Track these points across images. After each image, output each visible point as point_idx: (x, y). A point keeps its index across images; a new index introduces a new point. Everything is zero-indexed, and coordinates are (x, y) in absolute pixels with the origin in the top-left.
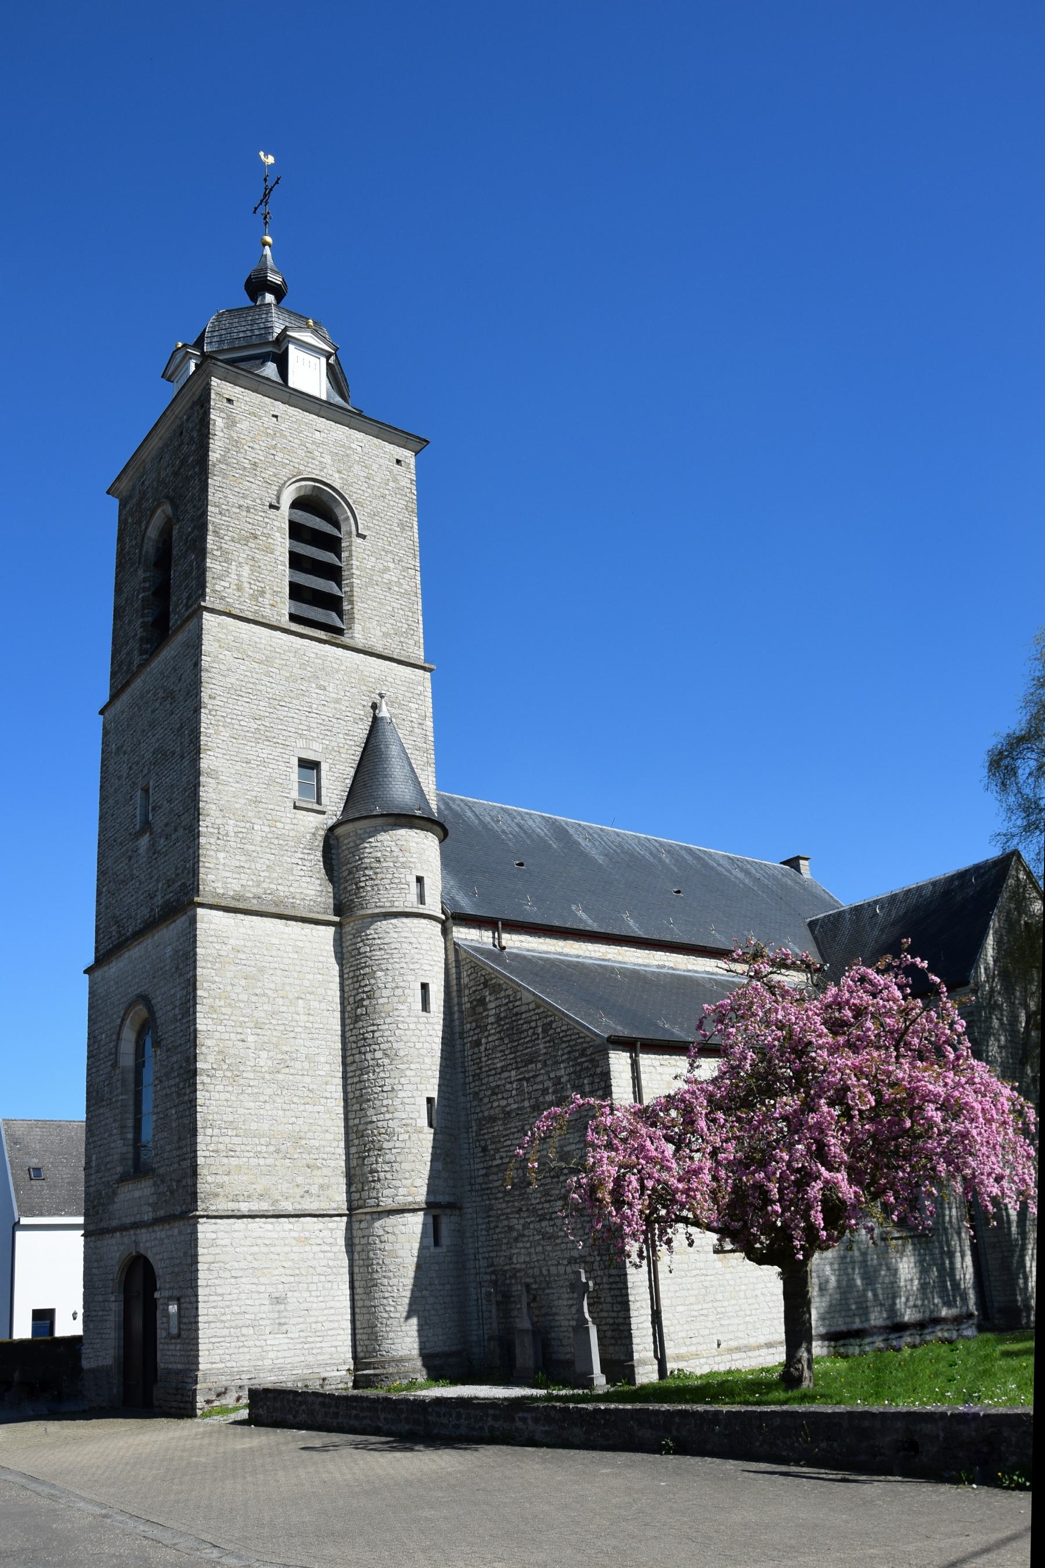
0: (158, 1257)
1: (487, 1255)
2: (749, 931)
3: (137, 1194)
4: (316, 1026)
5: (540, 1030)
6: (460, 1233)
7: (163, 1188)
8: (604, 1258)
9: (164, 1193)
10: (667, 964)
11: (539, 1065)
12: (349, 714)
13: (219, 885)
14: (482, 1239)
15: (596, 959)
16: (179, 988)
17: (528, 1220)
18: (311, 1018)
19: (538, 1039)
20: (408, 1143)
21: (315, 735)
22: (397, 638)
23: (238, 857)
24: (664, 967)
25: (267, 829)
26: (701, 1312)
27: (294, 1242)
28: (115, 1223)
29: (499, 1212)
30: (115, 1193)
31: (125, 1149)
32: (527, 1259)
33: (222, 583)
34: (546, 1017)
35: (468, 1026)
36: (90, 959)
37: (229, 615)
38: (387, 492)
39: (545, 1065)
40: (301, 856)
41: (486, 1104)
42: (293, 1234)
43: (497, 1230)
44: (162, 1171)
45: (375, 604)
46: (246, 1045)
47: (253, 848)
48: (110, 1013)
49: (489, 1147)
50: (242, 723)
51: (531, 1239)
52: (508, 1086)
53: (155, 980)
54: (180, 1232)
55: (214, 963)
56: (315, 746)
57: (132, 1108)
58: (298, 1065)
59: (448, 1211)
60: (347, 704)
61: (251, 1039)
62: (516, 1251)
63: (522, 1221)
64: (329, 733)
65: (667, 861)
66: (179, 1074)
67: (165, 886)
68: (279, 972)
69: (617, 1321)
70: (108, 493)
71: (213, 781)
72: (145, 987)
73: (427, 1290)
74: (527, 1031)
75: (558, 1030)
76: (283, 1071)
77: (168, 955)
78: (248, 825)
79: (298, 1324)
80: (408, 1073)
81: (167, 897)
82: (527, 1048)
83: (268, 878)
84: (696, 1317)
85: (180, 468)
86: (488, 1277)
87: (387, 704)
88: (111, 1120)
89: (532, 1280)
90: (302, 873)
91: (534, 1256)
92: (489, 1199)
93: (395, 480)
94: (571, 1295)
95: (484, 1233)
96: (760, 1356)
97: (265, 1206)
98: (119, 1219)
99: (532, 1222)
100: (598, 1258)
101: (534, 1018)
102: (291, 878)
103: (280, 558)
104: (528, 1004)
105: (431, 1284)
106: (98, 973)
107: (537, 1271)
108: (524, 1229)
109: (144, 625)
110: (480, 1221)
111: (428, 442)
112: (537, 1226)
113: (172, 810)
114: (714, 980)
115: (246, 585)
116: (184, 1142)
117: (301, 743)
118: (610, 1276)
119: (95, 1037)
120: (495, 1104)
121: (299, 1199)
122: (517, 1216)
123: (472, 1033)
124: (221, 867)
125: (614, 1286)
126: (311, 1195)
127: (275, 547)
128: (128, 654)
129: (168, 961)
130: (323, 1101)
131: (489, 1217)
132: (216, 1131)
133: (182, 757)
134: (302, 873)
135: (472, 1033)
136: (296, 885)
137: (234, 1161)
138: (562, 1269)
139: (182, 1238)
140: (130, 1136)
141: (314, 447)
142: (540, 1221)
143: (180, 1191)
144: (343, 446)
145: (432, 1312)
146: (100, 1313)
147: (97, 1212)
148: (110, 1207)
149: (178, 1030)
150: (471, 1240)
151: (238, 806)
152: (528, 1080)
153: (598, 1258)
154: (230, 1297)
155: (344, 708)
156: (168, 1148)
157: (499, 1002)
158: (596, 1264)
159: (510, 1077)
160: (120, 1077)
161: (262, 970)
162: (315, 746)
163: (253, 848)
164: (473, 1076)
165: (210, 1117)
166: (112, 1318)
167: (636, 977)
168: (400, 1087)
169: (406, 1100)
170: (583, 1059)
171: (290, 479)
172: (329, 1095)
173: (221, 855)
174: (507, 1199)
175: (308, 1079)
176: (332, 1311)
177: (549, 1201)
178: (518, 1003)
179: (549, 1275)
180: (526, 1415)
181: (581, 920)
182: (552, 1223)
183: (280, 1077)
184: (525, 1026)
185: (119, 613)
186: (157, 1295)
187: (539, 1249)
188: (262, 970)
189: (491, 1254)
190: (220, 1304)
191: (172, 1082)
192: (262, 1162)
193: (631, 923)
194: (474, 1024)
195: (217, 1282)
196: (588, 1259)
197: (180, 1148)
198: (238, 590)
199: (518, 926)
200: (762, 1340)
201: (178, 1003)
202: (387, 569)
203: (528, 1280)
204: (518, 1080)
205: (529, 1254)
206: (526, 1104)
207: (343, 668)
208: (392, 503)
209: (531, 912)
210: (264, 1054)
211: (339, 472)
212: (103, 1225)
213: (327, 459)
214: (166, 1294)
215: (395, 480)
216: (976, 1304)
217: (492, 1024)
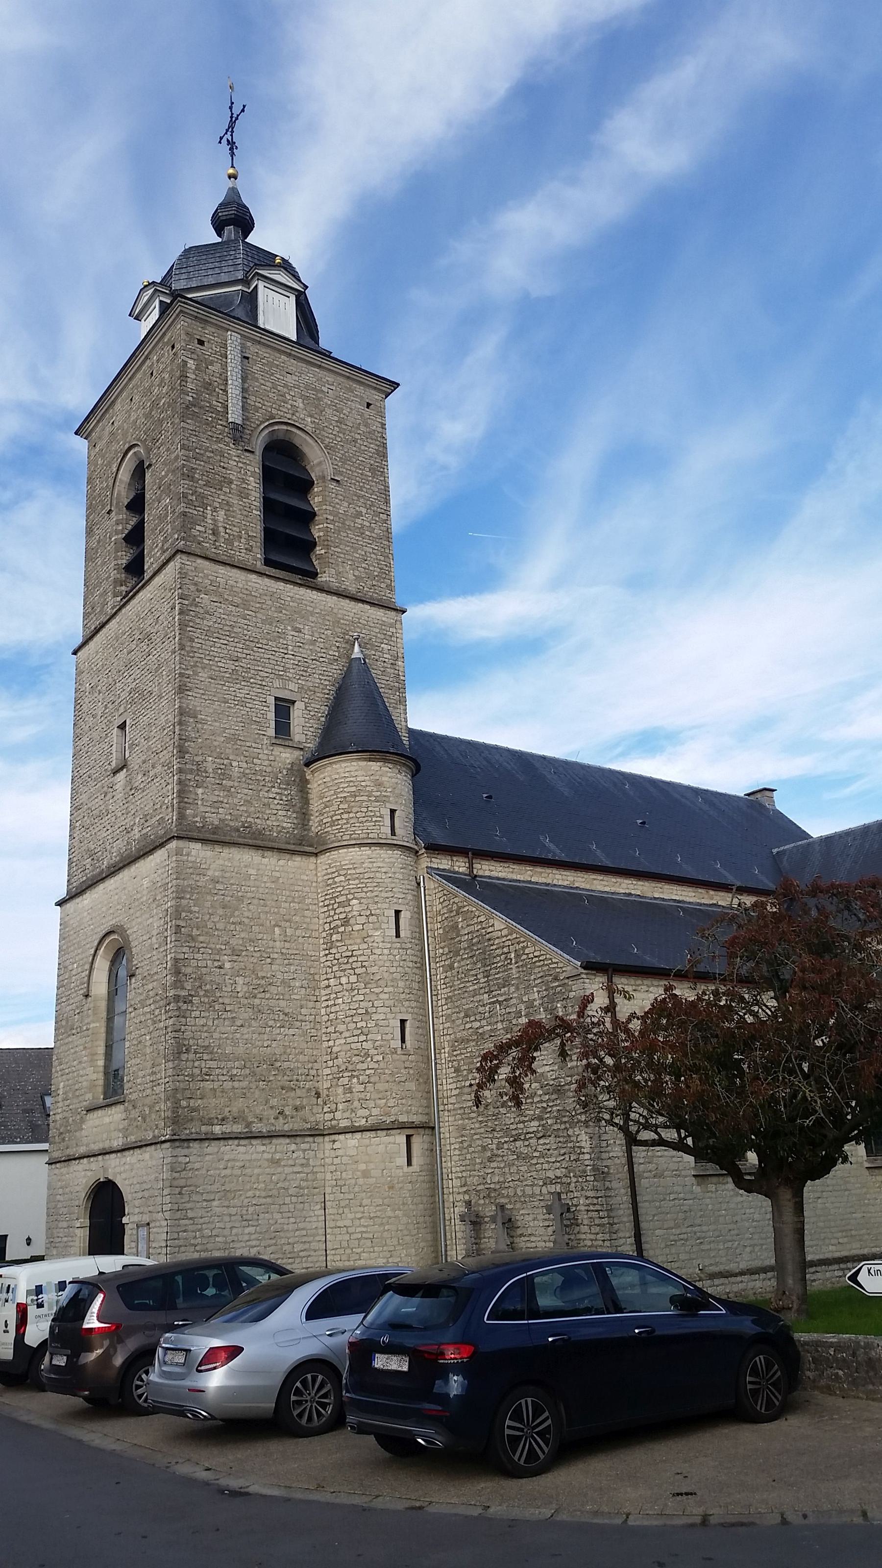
0: (127, 1182)
2: (715, 861)
3: (107, 1120)
4: (290, 952)
5: (513, 955)
7: (135, 1114)
9: (135, 1119)
10: (633, 892)
11: (512, 989)
12: (324, 655)
13: (198, 819)
14: (456, 1158)
15: (565, 887)
16: (156, 918)
18: (287, 945)
19: (510, 964)
20: (382, 1065)
21: (291, 675)
22: (369, 582)
23: (216, 793)
24: (630, 894)
25: (244, 765)
26: (682, 1236)
27: (266, 1164)
28: (82, 1150)
30: (82, 1121)
31: (94, 1076)
32: (502, 1179)
33: (198, 528)
34: (518, 943)
35: (441, 951)
36: (63, 893)
37: (206, 558)
38: (358, 437)
39: (517, 989)
40: (278, 791)
41: (458, 1026)
42: (266, 1156)
44: (133, 1097)
45: (348, 548)
46: (223, 971)
47: (230, 783)
48: (83, 943)
49: (462, 1068)
50: (220, 664)
52: (481, 1009)
53: (132, 911)
54: (151, 1157)
55: (192, 894)
56: (292, 686)
57: (103, 1036)
58: (273, 989)
59: (422, 1131)
60: (322, 645)
61: (228, 965)
63: (495, 1141)
64: (304, 674)
65: (631, 793)
66: (154, 1002)
67: (142, 821)
68: (255, 901)
70: (76, 433)
71: (192, 720)
72: (121, 918)
74: (500, 956)
75: (531, 956)
76: (259, 996)
77: (145, 886)
78: (226, 762)
79: (269, 1246)
80: (382, 996)
81: (144, 831)
82: (499, 973)
83: (246, 812)
84: (675, 1241)
85: (151, 410)
86: (461, 1197)
87: (360, 646)
88: (81, 1048)
89: (507, 1201)
90: (279, 807)
91: (508, 1176)
92: (463, 1119)
93: (367, 425)
94: (547, 1216)
95: (457, 1152)
96: (742, 1282)
97: (238, 1128)
98: (87, 1145)
99: (506, 1142)
100: (574, 1180)
101: (507, 943)
102: (268, 812)
103: (254, 503)
104: (500, 930)
105: (404, 1204)
106: (69, 906)
107: (511, 1192)
108: (498, 1149)
109: (117, 567)
111: (398, 385)
113: (149, 748)
114: (681, 907)
115: (221, 529)
116: (158, 1068)
117: (277, 684)
118: (587, 1198)
119: (65, 967)
120: (468, 1026)
121: (273, 1121)
123: (444, 958)
124: (200, 803)
125: (592, 1208)
126: (286, 1117)
127: (250, 492)
128: (101, 595)
129: (145, 892)
130: (299, 1024)
131: (462, 1136)
132: (191, 1056)
133: (160, 697)
134: (279, 807)
135: (444, 958)
136: (273, 818)
137: (208, 1085)
138: (537, 1190)
139: (154, 1163)
140: (101, 1063)
141: (285, 390)
142: (515, 1140)
143: (153, 1116)
144: (315, 389)
145: (405, 1232)
146: (65, 1239)
147: (63, 1140)
148: (77, 1134)
149: (155, 958)
151: (216, 743)
152: (500, 1003)
153: (574, 1180)
154: (202, 1221)
155: (319, 650)
156: (141, 1074)
157: (471, 928)
158: (573, 1185)
159: (483, 1000)
160: (92, 1005)
161: (240, 899)
162: (292, 686)
163: (230, 783)
164: (446, 999)
165: (186, 1043)
166: (77, 1244)
167: (602, 902)
168: (374, 1010)
169: (381, 1023)
170: (556, 984)
171: (262, 422)
172: (303, 1018)
173: (200, 791)
174: (480, 1119)
175: (283, 1003)
176: (304, 1233)
177: (524, 1122)
178: (491, 929)
179: (524, 1195)
181: (549, 851)
182: (527, 1143)
183: (257, 1001)
184: (499, 952)
185: (90, 556)
186: (125, 1220)
187: (514, 1169)
188: (240, 899)
190: (190, 1228)
191: (147, 1009)
192: (236, 1084)
193: (598, 852)
194: (446, 950)
195: (188, 1206)
196: (564, 1180)
197: (154, 1073)
198: (214, 534)
199: (487, 856)
200: (743, 1266)
201: (155, 933)
202: (360, 514)
203: (503, 1201)
204: (490, 1003)
206: (500, 1026)
207: (318, 611)
208: (363, 447)
209: (500, 841)
210: (240, 980)
211: (311, 416)
212: (70, 1152)
213: (300, 403)
214: (136, 1218)
215: (367, 425)
217: (465, 949)
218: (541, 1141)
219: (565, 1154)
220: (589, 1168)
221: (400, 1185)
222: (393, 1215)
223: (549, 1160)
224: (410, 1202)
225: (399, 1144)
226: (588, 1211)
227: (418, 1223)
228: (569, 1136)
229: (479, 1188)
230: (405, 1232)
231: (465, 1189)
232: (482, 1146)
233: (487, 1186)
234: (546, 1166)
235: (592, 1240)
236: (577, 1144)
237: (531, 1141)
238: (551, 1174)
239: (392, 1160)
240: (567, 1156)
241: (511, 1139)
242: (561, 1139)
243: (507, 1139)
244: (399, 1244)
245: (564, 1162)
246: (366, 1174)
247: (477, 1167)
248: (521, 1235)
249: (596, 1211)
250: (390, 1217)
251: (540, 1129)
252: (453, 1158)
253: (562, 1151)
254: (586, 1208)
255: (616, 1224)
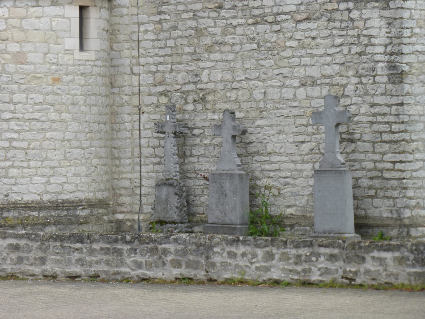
1: (153, 68)
6: (111, 33)
8: (364, 80)
17: (235, 22)
29: (181, 8)
32: (228, 77)
43: (175, 34)
51: (237, 48)
62: (208, 64)
63: (221, 23)
69: (380, 166)
73: (68, 112)
91: (240, 73)
95: (150, 36)
99: (240, 25)
105: (74, 104)
108: (224, 34)
110: (143, 18)
112: (250, 31)
118: (373, 105)
122: (214, 15)
131: (160, 13)
142: (256, 24)
150: (127, 45)
153: (355, 80)
180: (384, 255)
182: (276, 27)
189: (161, 68)
196: (338, 80)
205: (232, 70)
216: (420, 241)
218: (304, 25)
219: (341, 45)
220: (380, 65)
221: (70, 78)
222: (57, 118)
223: (314, 52)
224: (81, 102)
225: (69, 19)
226: (372, 123)
227: (91, 132)
228: (352, 20)
229: (187, 88)
230: (75, 143)
231: (160, 89)
232: (196, 29)
233: (200, 86)
234: (307, 60)
235: (375, 162)
236: (365, 32)
237: (284, 25)
238: (314, 72)
239: (59, 41)
240: (345, 49)
241: (250, 21)
242: (338, 24)
243: (241, 21)
244: (65, 159)
245: (339, 56)
246: (20, 58)
247: (186, 58)
248: (257, 153)
249: (387, 123)
250: (54, 121)
251: (302, 8)
252: (143, 44)
253: (338, 41)
254: (371, 119)
255: (413, 141)
